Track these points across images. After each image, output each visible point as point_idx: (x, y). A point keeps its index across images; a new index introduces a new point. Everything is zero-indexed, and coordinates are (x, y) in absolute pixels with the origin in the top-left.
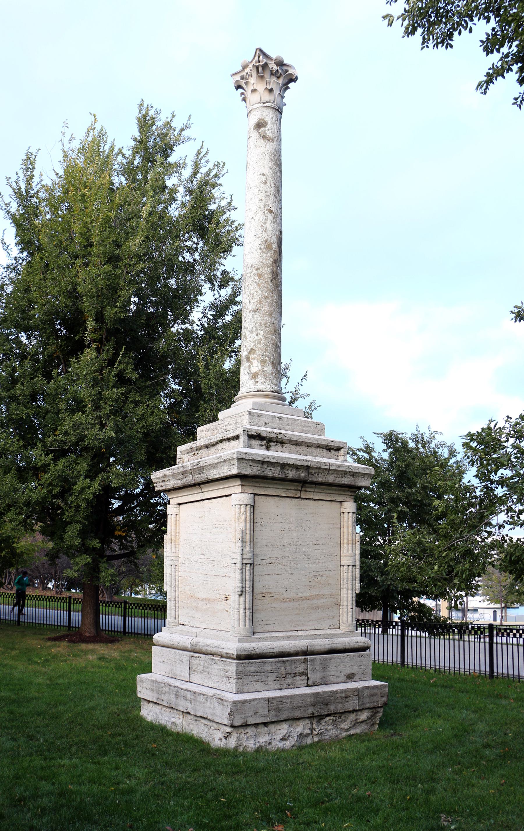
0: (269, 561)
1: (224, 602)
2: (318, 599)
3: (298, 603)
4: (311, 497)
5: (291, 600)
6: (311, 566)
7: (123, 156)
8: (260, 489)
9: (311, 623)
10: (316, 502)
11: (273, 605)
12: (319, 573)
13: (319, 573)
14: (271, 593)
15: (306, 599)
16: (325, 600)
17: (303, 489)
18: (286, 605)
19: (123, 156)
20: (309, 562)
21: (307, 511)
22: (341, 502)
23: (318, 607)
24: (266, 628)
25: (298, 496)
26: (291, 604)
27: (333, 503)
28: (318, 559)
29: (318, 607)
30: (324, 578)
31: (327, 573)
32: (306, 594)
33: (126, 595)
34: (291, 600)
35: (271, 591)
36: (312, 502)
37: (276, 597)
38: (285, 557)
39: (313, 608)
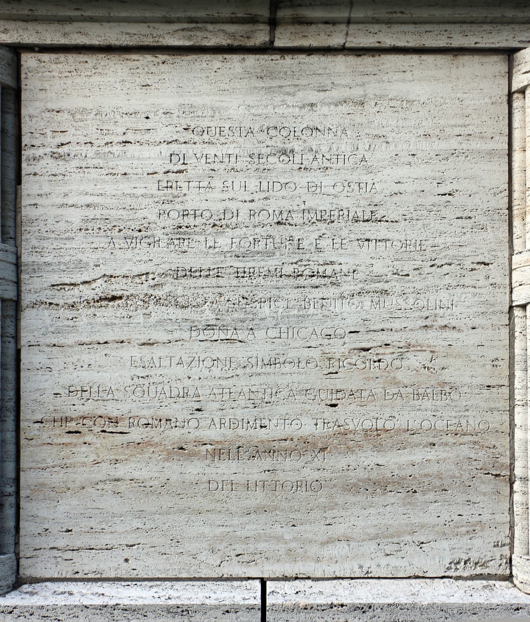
0: (101, 288)
1: (519, 558)
2: (378, 448)
3: (267, 463)
4: (336, 41)
5: (220, 452)
6: (338, 307)
7: (11, 238)
8: (40, 27)
9: (340, 549)
10: (368, 60)
11: (121, 471)
12: (383, 338)
13: (383, 338)
14: (115, 421)
15: (307, 446)
16: (419, 455)
17: (283, 13)
18: (194, 469)
19: (11, 238)
20: (331, 292)
21: (313, 96)
22: (509, 54)
23: (380, 485)
24: (87, 564)
25: (261, 37)
26: (226, 469)
27: (465, 59)
28: (378, 278)
29: (380, 485)
30: (414, 360)
31: (432, 338)
32: (307, 428)
33: (19, 29)
34: (220, 452)
35: (112, 409)
36: (340, 63)
37: (136, 434)
38: (190, 273)
39: (353, 488)
